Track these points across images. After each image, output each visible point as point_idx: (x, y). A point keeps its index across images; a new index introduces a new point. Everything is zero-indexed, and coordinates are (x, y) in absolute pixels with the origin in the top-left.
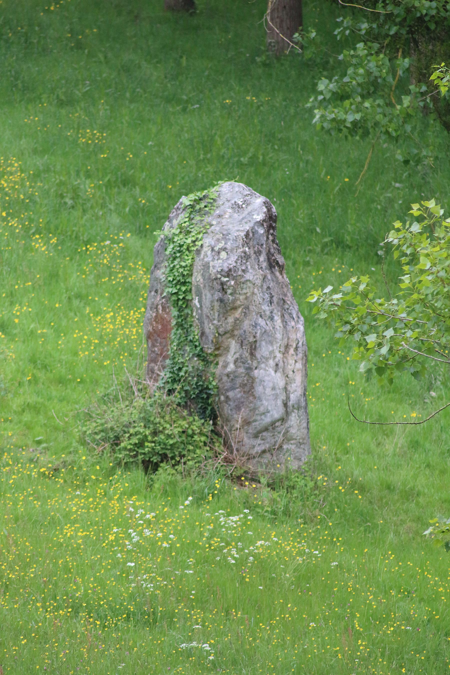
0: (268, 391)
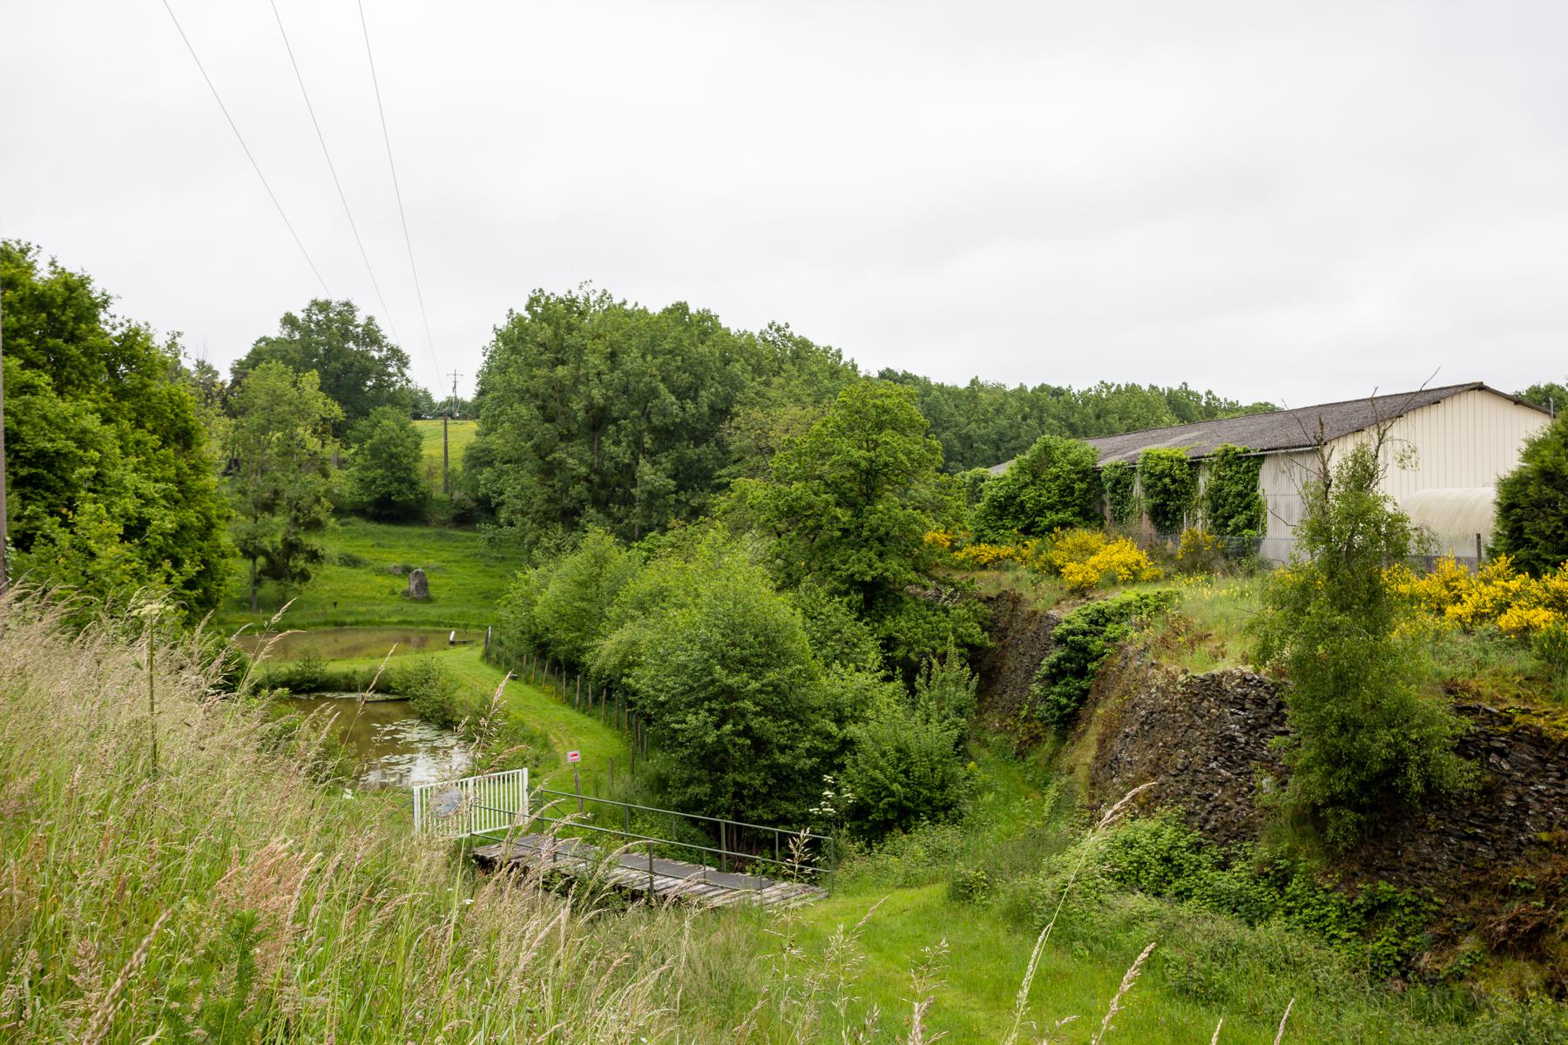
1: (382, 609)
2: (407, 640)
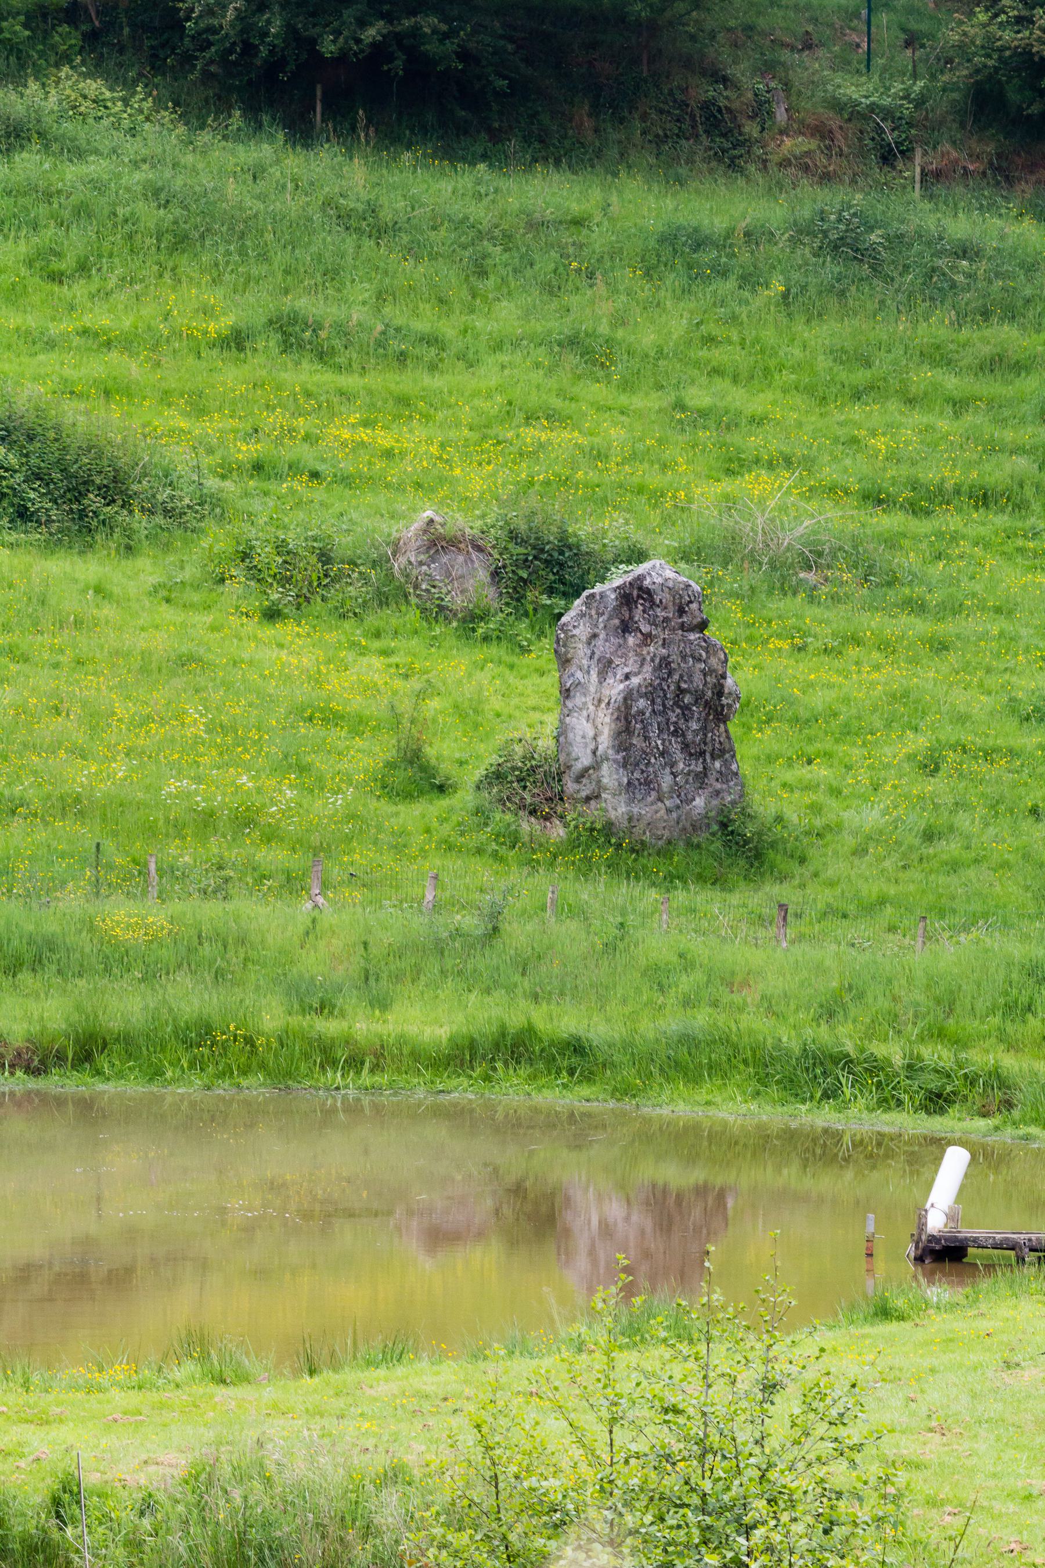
0: (578, 739)
1: (318, 929)
2: (536, 1219)
